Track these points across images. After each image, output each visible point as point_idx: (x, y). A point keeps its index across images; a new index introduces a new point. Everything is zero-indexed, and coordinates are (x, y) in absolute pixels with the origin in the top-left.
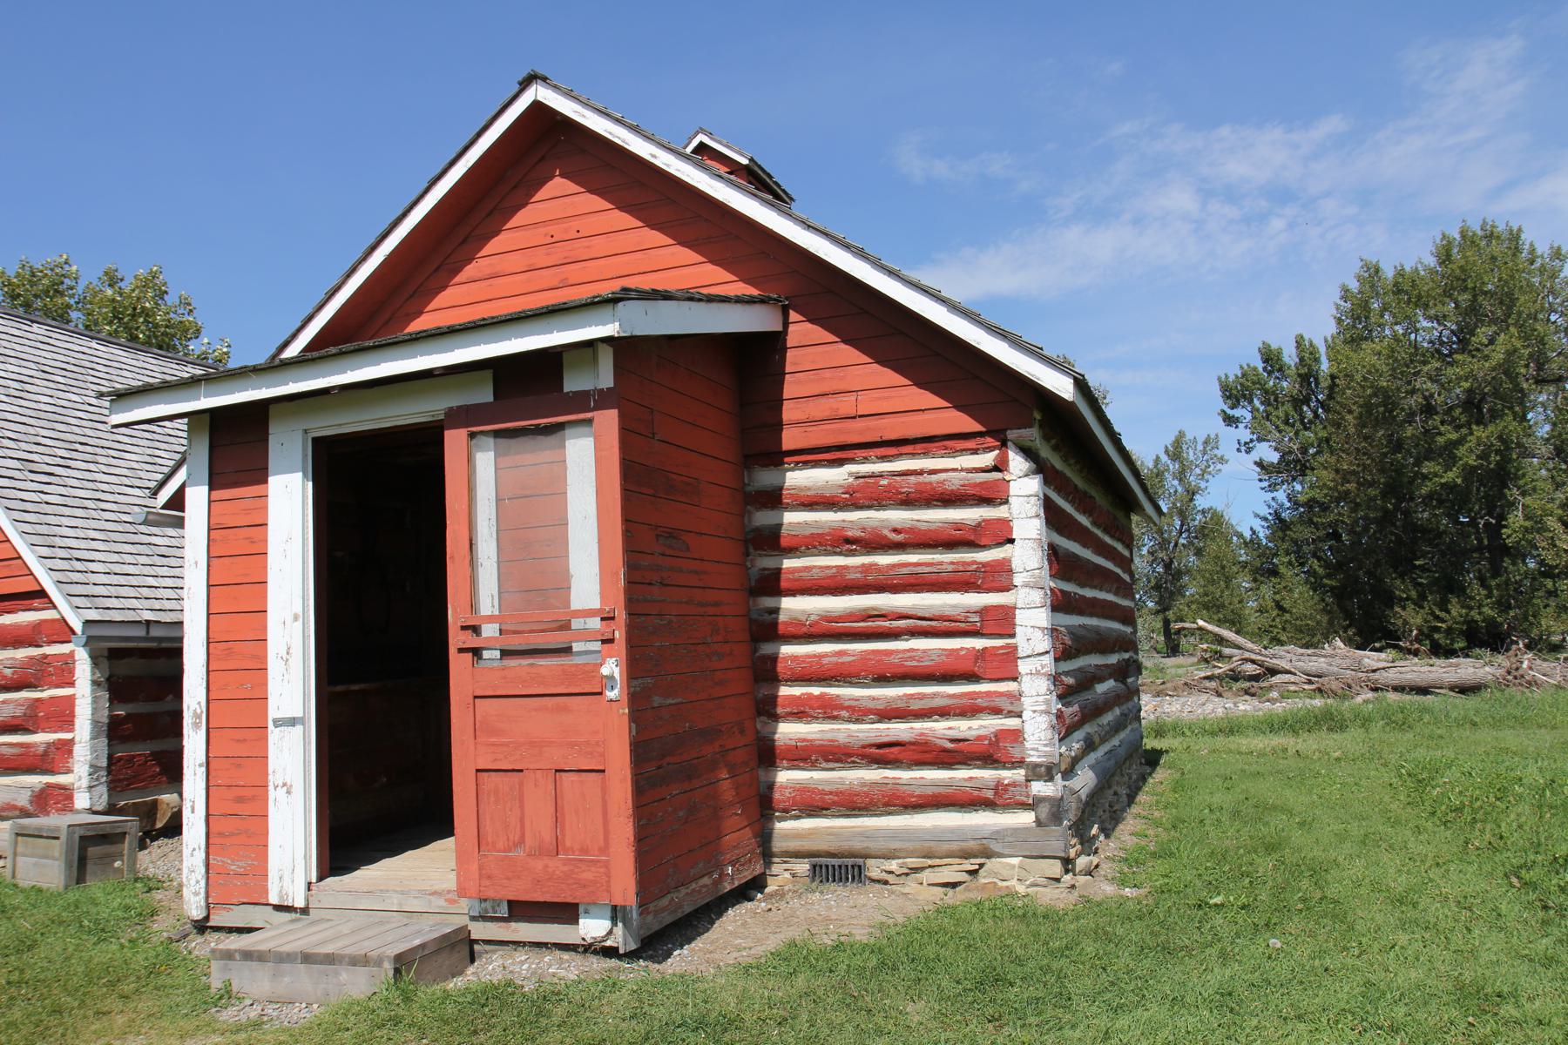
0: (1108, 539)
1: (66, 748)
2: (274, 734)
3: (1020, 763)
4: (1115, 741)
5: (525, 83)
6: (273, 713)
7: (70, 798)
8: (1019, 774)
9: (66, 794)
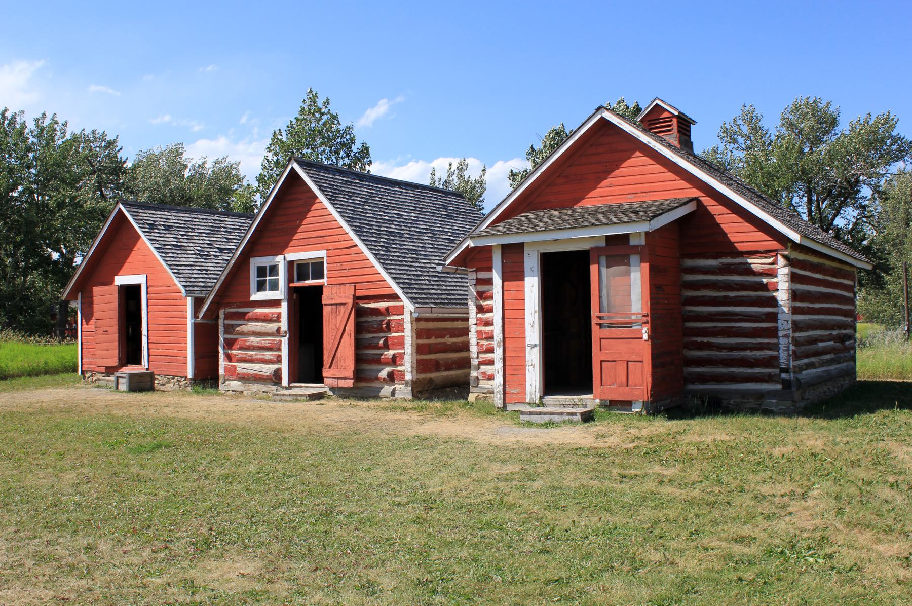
0: (835, 280)
1: (402, 356)
2: (528, 349)
3: (778, 367)
4: (832, 368)
5: (599, 109)
6: (527, 342)
7: (404, 375)
8: (777, 371)
9: (402, 374)
